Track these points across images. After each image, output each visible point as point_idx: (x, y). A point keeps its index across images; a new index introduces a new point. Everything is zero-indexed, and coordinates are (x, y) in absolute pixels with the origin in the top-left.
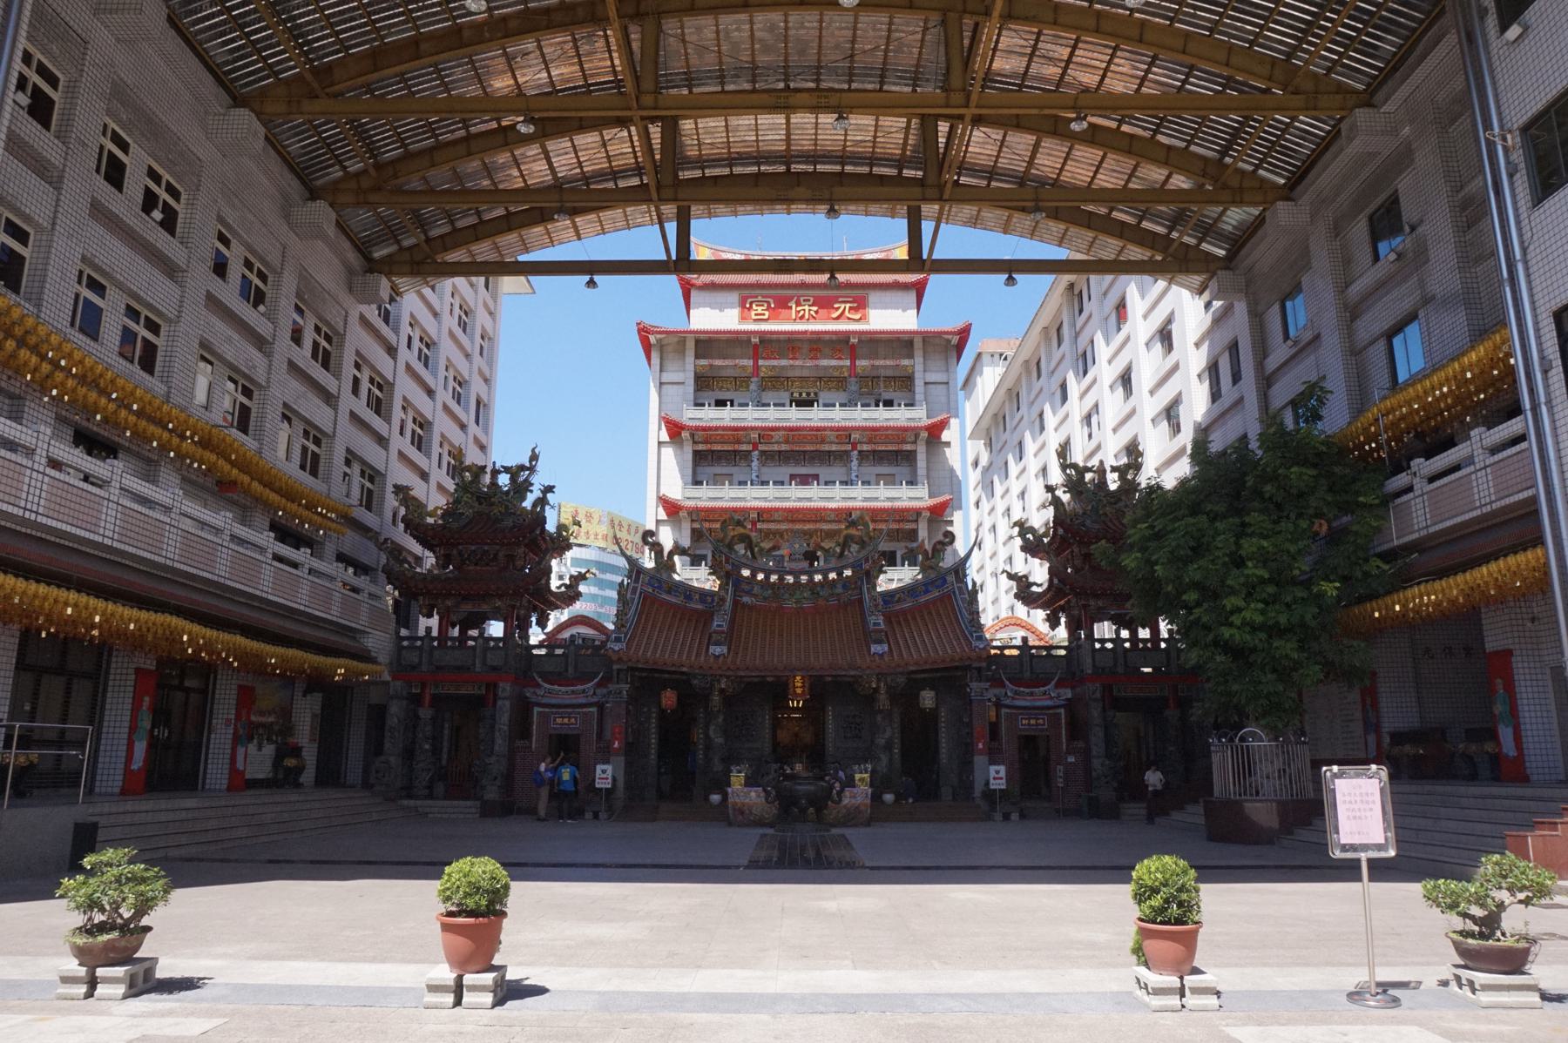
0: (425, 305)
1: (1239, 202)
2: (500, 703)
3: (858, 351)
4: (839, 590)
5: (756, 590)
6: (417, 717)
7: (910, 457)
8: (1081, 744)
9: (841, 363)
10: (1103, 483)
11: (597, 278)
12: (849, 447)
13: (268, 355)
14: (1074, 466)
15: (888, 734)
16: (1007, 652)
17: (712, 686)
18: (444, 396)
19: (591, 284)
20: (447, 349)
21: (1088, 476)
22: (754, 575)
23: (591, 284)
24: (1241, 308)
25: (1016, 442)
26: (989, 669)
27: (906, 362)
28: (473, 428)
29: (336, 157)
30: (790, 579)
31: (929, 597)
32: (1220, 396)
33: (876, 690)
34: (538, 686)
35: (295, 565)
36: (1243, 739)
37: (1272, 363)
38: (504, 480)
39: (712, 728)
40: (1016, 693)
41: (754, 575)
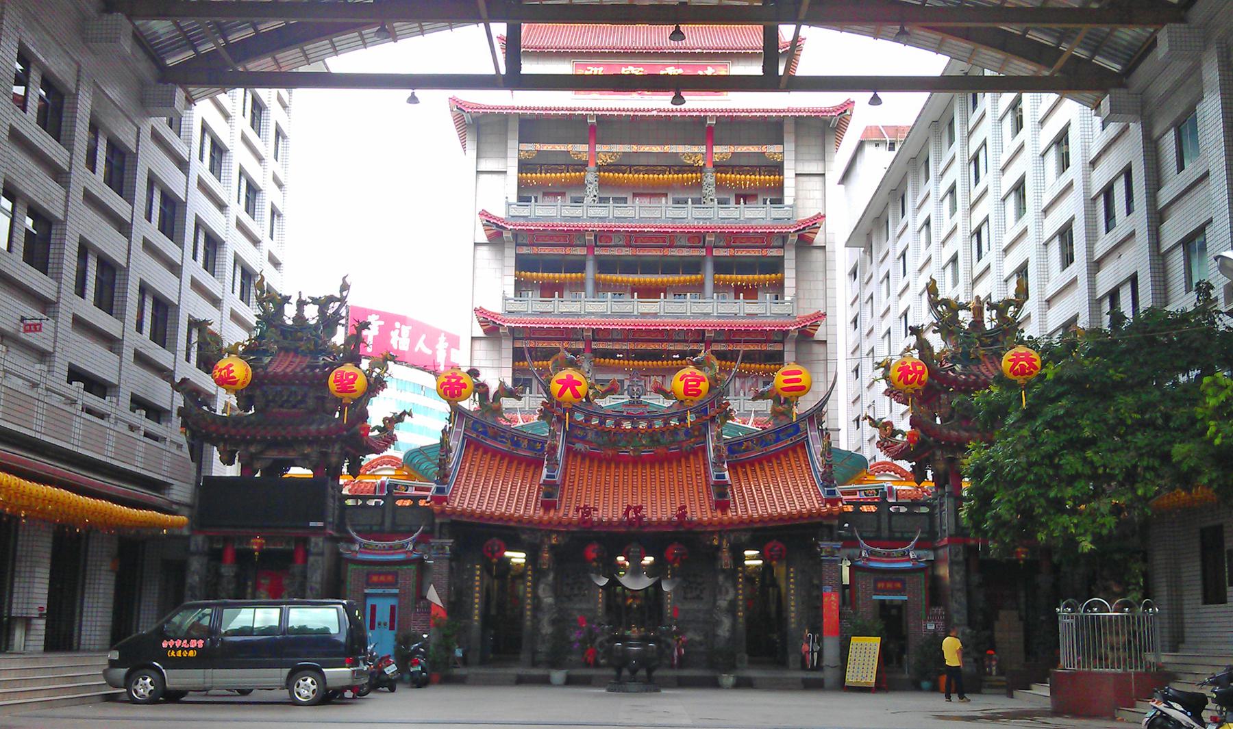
0: (217, 113)
1: (1129, 22)
2: (311, 559)
3: (716, 134)
4: (682, 437)
5: (591, 436)
6: (218, 575)
7: (776, 266)
8: (940, 610)
9: (695, 149)
10: (978, 323)
11: (419, 93)
12: (703, 252)
13: (179, 276)
14: (946, 302)
15: (730, 596)
16: (865, 508)
17: (542, 542)
18: (237, 209)
19: (413, 100)
20: (238, 156)
21: (962, 314)
22: (588, 420)
23: (413, 100)
24: (1136, 129)
25: (899, 252)
26: (841, 527)
27: (774, 148)
28: (267, 244)
29: (188, 38)
30: (627, 425)
31: (781, 445)
32: (1072, 261)
33: (719, 548)
34: (353, 541)
35: (102, 416)
36: (1089, 606)
37: (1165, 196)
38: (311, 312)
39: (542, 586)
40: (871, 553)
41: (588, 420)
